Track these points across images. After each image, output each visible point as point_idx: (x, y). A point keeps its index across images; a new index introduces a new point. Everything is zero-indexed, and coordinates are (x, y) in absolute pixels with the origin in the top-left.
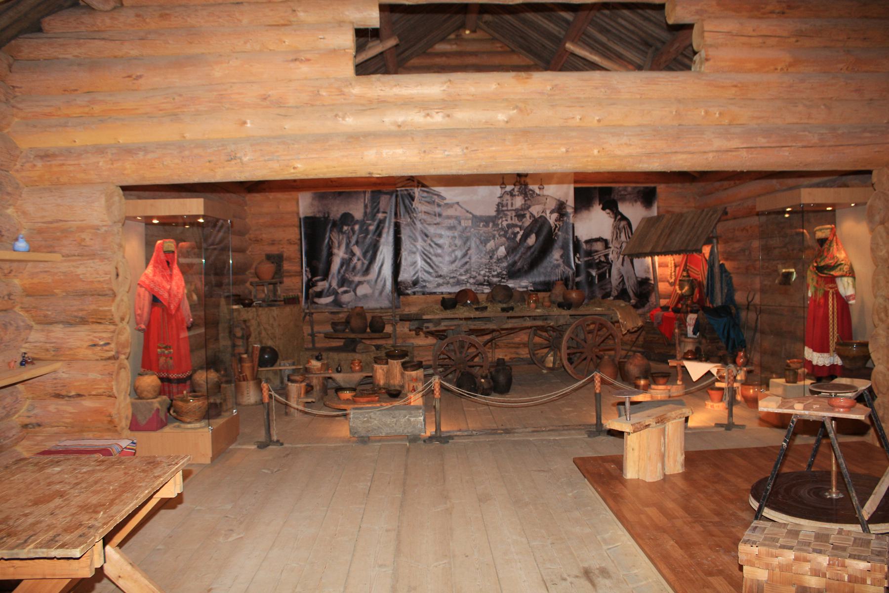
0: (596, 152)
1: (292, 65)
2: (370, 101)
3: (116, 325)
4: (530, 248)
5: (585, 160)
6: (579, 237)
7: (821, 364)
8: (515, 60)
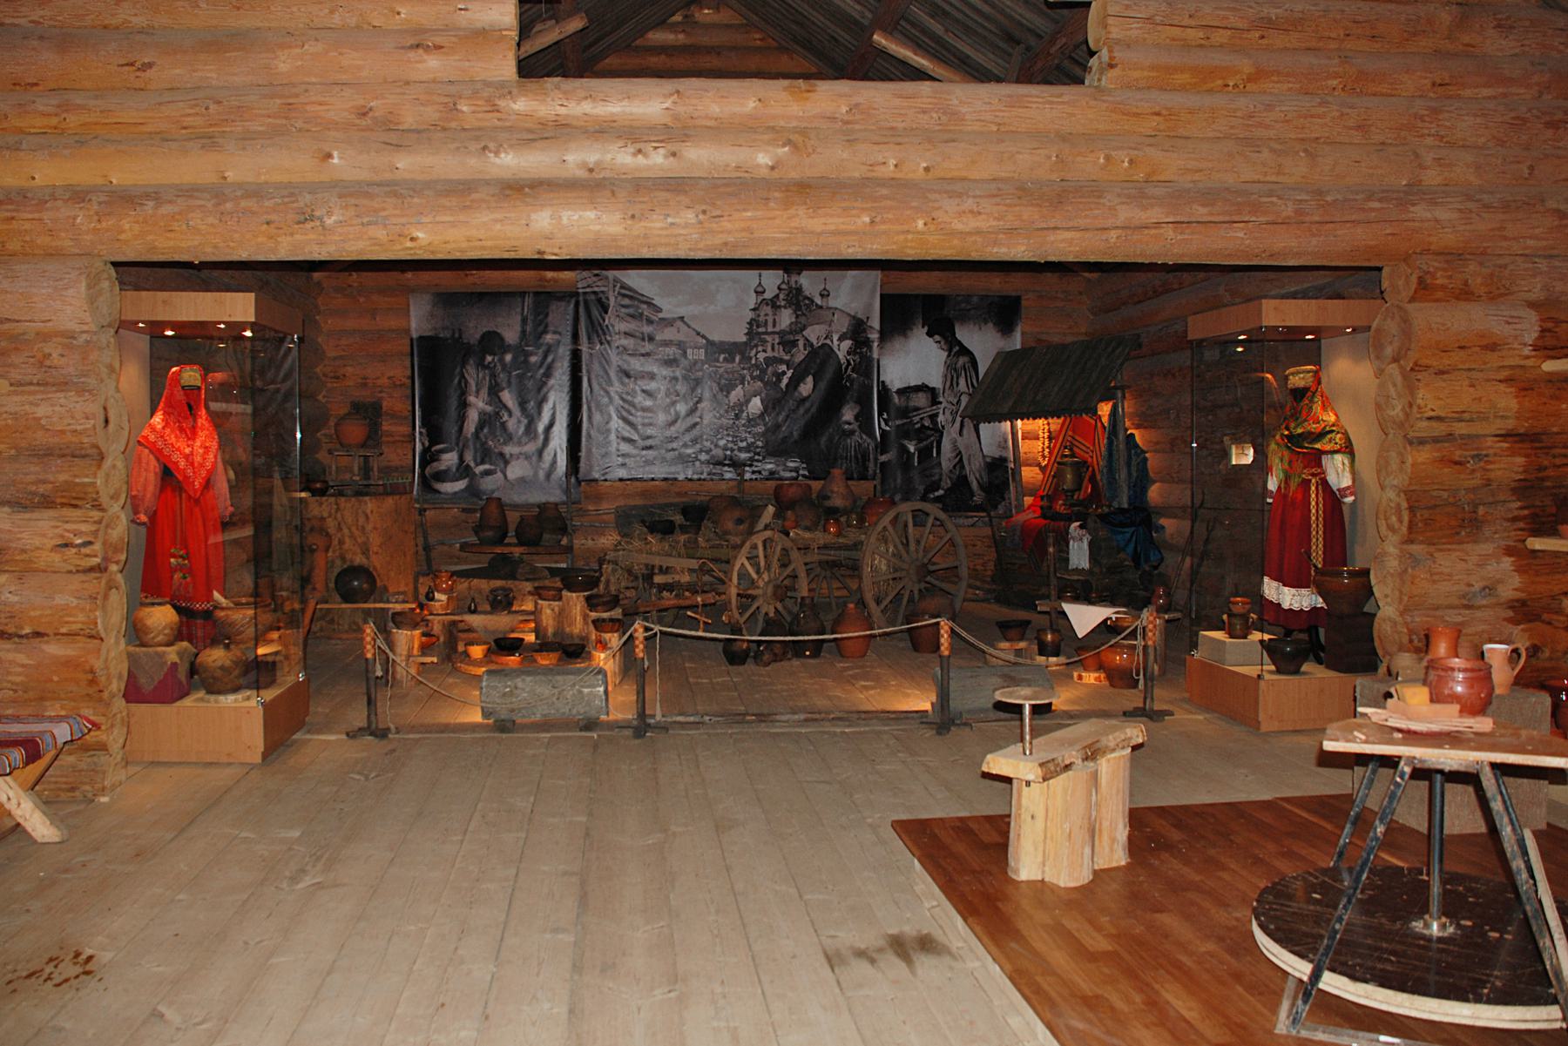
0: (920, 224)
1: (412, 55)
2: (543, 124)
3: (103, 510)
4: (804, 400)
5: (902, 237)
6: (888, 382)
7: (1296, 607)
8: (785, 63)
